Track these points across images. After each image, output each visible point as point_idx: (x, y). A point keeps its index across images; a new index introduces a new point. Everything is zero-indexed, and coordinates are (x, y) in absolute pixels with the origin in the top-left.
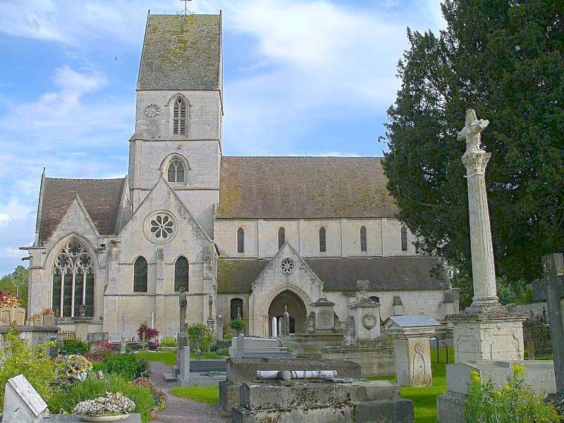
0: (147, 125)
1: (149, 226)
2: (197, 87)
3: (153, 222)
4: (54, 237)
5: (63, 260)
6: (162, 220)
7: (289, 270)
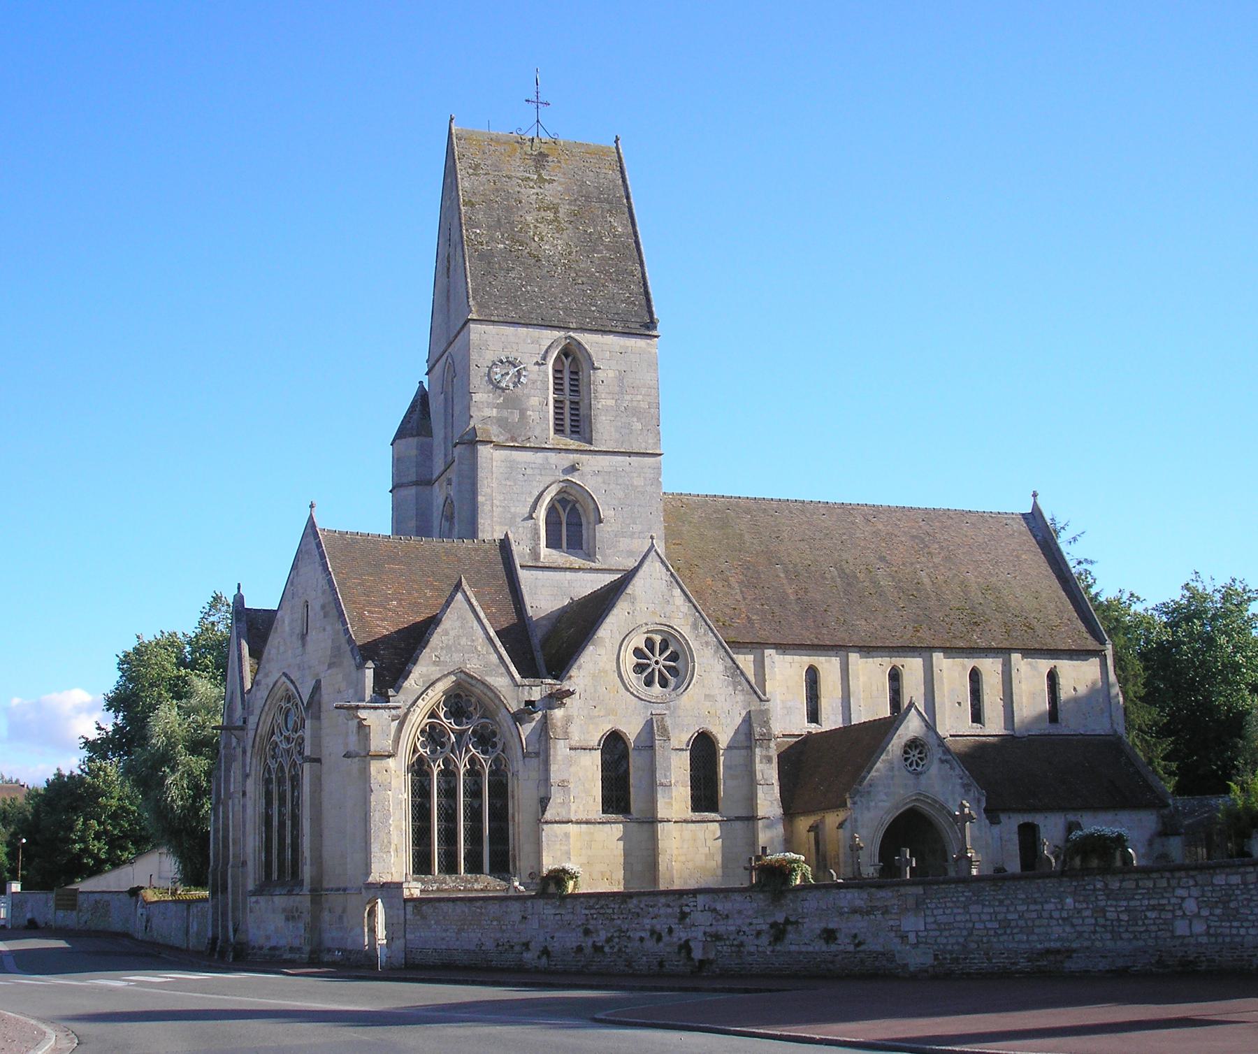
0: (498, 406)
1: (629, 660)
2: (610, 325)
3: (638, 652)
4: (413, 682)
5: (433, 735)
6: (646, 650)
7: (918, 765)
